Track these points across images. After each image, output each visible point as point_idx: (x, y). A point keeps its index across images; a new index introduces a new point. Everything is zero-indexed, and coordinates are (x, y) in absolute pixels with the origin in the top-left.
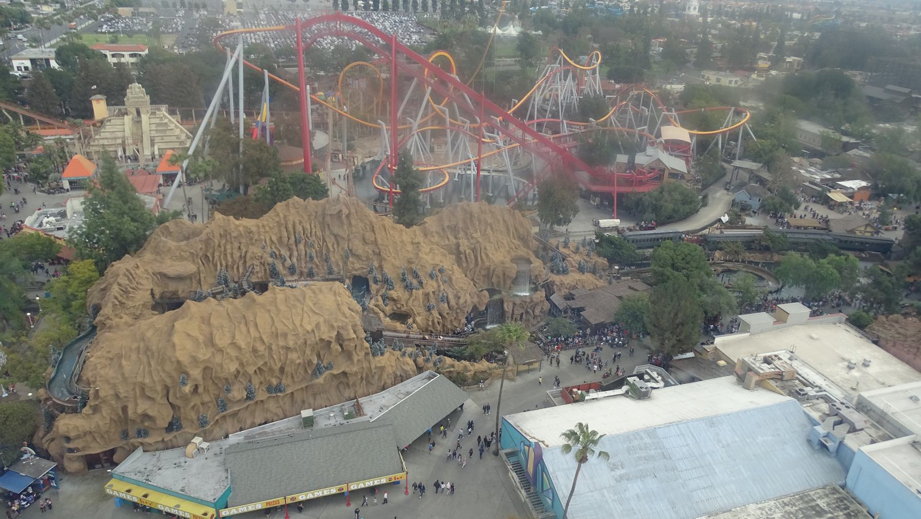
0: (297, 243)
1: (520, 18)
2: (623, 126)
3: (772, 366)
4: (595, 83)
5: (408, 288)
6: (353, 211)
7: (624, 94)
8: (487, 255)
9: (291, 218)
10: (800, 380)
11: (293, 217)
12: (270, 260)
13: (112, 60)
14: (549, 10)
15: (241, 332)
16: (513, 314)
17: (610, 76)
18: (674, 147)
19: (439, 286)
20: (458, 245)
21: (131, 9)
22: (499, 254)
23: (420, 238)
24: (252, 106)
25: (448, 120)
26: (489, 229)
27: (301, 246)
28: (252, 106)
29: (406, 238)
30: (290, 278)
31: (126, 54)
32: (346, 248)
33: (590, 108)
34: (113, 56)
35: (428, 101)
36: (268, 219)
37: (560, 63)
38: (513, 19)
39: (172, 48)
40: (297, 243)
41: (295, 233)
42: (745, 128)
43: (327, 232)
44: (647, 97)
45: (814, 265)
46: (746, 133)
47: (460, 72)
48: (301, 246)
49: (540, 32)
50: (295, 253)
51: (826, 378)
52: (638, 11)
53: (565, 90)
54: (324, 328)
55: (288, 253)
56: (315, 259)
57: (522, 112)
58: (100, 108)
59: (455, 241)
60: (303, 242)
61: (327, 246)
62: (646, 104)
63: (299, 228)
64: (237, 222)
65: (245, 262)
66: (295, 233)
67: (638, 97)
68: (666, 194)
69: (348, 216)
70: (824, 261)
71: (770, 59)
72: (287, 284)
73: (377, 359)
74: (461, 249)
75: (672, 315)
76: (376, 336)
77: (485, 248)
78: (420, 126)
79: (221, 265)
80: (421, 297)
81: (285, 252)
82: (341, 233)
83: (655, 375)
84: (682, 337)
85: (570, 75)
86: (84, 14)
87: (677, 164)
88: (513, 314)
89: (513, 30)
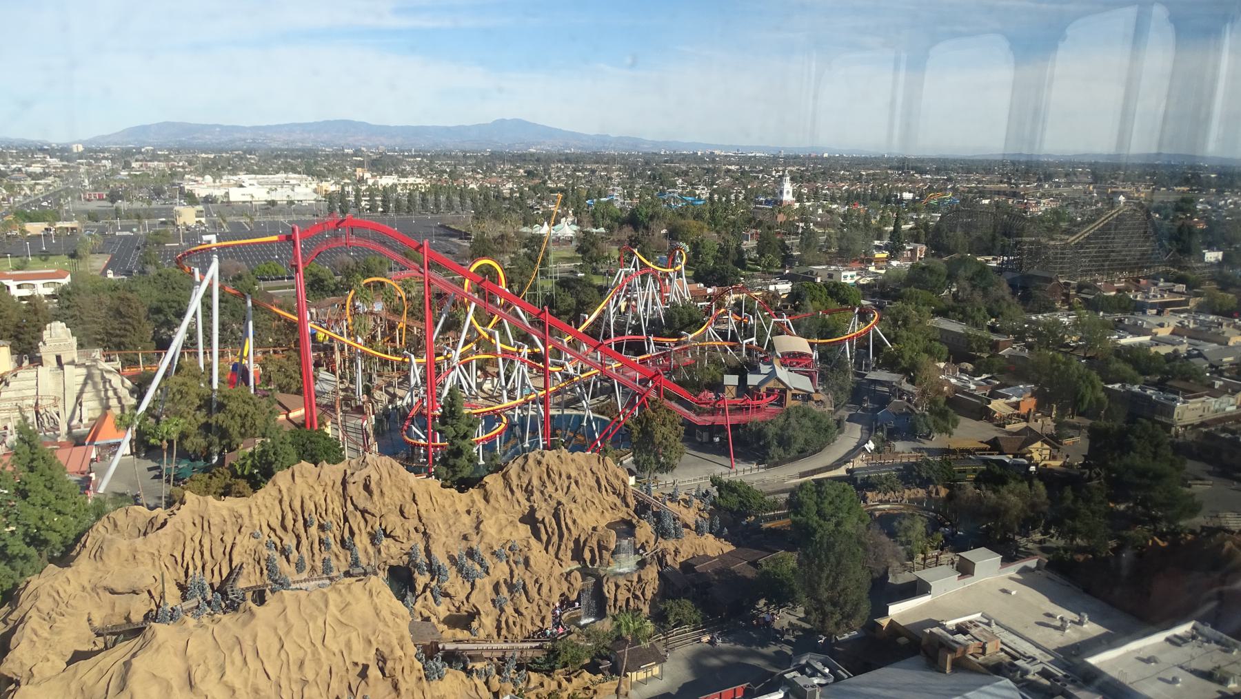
0: (306, 525)
1: (575, 214)
2: (725, 339)
3: (969, 636)
4: (681, 288)
5: (466, 575)
6: (385, 475)
7: (718, 300)
8: (574, 522)
9: (298, 493)
10: (1006, 652)
11: (301, 488)
12: (266, 552)
13: (15, 292)
14: (610, 202)
15: (233, 663)
16: (616, 600)
17: (696, 278)
18: (792, 360)
19: (512, 572)
20: (533, 510)
21: (46, 225)
22: (592, 516)
23: (481, 504)
25: (499, 346)
26: (573, 485)
27: (314, 530)
29: (461, 508)
30: (297, 578)
31: (39, 283)
32: (377, 527)
33: (676, 322)
34: (19, 287)
35: (471, 323)
36: (267, 494)
37: (635, 266)
38: (565, 215)
39: (104, 273)
40: (306, 525)
41: (303, 512)
42: (875, 332)
43: (350, 507)
44: (751, 300)
45: (993, 496)
46: (877, 340)
47: (510, 284)
48: (314, 530)
49: (602, 230)
50: (304, 542)
51: (1038, 646)
52: (720, 199)
53: (648, 302)
54: (357, 646)
55: (295, 542)
56: (333, 546)
57: (593, 332)
58: (1109, 530)
59: (528, 504)
60: (316, 523)
61: (350, 528)
62: (751, 312)
63: (310, 506)
64: (218, 504)
65: (231, 560)
66: (303, 512)
67: (738, 303)
68: (792, 420)
69: (379, 483)
70: (1004, 490)
71: (886, 248)
72: (293, 586)
73: (434, 683)
74: (539, 515)
75: (831, 580)
76: (429, 652)
77: (571, 512)
78: (462, 356)
79: (195, 569)
80: (489, 589)
81: (290, 541)
82: (369, 507)
83: (819, 666)
84: (847, 609)
85: (650, 280)
86: (919, 476)
87: (802, 383)
88: (616, 600)
89: (567, 229)
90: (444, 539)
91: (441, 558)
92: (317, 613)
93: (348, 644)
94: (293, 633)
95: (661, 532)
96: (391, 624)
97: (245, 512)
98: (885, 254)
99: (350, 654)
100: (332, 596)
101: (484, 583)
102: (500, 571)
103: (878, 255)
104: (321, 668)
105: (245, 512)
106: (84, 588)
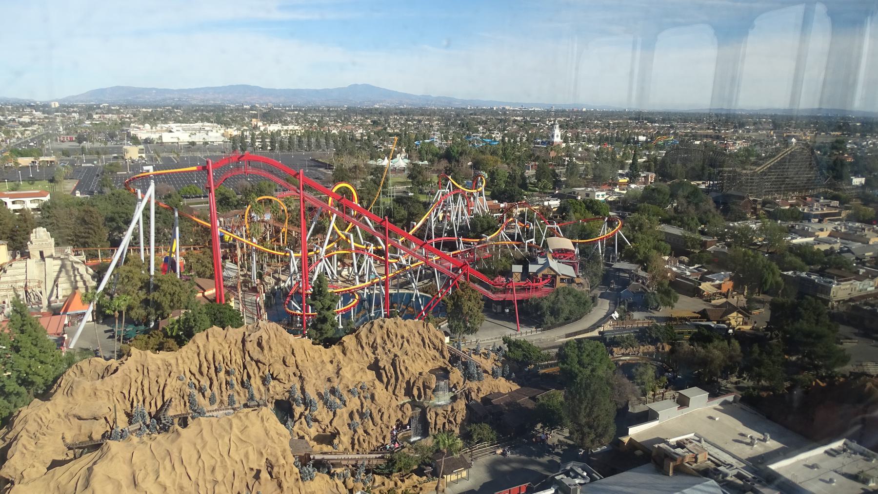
0: (217, 371)
1: (407, 151)
2: (513, 240)
3: (685, 450)
4: (482, 204)
5: (330, 406)
6: (272, 335)
7: (508, 212)
8: (406, 369)
9: (211, 349)
10: (712, 461)
11: (213, 345)
12: (188, 390)
13: (11, 207)
14: (432, 143)
15: (165, 469)
16: (436, 424)
17: (493, 197)
18: (560, 254)
19: (362, 404)
20: (377, 361)
21: (32, 159)
22: (419, 365)
23: (340, 356)
24: (164, 239)
25: (353, 244)
26: (406, 343)
27: (222, 374)
28: (164, 239)
29: (326, 359)
30: (210, 408)
31: (27, 200)
32: (267, 372)
33: (479, 227)
34: (14, 203)
35: (333, 228)
36: (189, 349)
37: (449, 188)
38: (400, 152)
39: (74, 193)
40: (217, 371)
41: (214, 362)
42: (619, 235)
43: (248, 358)
44: (531, 212)
45: (702, 351)
46: (621, 240)
47: (361, 201)
48: (222, 374)
49: (426, 162)
50: (215, 383)
51: (734, 457)
52: (509, 141)
53: (458, 213)
54: (253, 456)
55: (208, 383)
56: (236, 386)
57: (420, 235)
59: (373, 356)
60: (224, 370)
61: (248, 373)
62: (531, 220)
63: (219, 357)
64: (155, 356)
65: (163, 396)
66: (214, 362)
67: (522, 214)
68: (561, 297)
69: (268, 342)
70: (710, 346)
71: (627, 175)
72: (207, 414)
73: (307, 483)
74: (381, 364)
75: (588, 410)
76: (304, 461)
77: (404, 362)
78: (327, 252)
79: (138, 402)
80: (346, 416)
81: (205, 382)
82: (261, 358)
83: (579, 471)
84: (600, 430)
85: (460, 198)
87: (567, 271)
88: (436, 424)
89: (401, 162)
90: (314, 381)
91: (312, 394)
92: (224, 433)
93: (247, 455)
94: (208, 447)
95: (468, 376)
96: (276, 441)
97: (173, 362)
98: (626, 180)
99: (248, 462)
100: (235, 421)
101: (343, 412)
102: (354, 403)
103: (621, 180)
104: (227, 472)
105: (173, 362)
106: (59, 416)
